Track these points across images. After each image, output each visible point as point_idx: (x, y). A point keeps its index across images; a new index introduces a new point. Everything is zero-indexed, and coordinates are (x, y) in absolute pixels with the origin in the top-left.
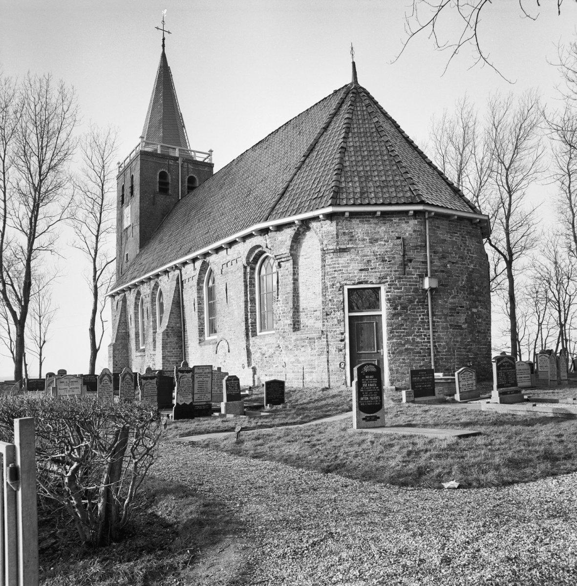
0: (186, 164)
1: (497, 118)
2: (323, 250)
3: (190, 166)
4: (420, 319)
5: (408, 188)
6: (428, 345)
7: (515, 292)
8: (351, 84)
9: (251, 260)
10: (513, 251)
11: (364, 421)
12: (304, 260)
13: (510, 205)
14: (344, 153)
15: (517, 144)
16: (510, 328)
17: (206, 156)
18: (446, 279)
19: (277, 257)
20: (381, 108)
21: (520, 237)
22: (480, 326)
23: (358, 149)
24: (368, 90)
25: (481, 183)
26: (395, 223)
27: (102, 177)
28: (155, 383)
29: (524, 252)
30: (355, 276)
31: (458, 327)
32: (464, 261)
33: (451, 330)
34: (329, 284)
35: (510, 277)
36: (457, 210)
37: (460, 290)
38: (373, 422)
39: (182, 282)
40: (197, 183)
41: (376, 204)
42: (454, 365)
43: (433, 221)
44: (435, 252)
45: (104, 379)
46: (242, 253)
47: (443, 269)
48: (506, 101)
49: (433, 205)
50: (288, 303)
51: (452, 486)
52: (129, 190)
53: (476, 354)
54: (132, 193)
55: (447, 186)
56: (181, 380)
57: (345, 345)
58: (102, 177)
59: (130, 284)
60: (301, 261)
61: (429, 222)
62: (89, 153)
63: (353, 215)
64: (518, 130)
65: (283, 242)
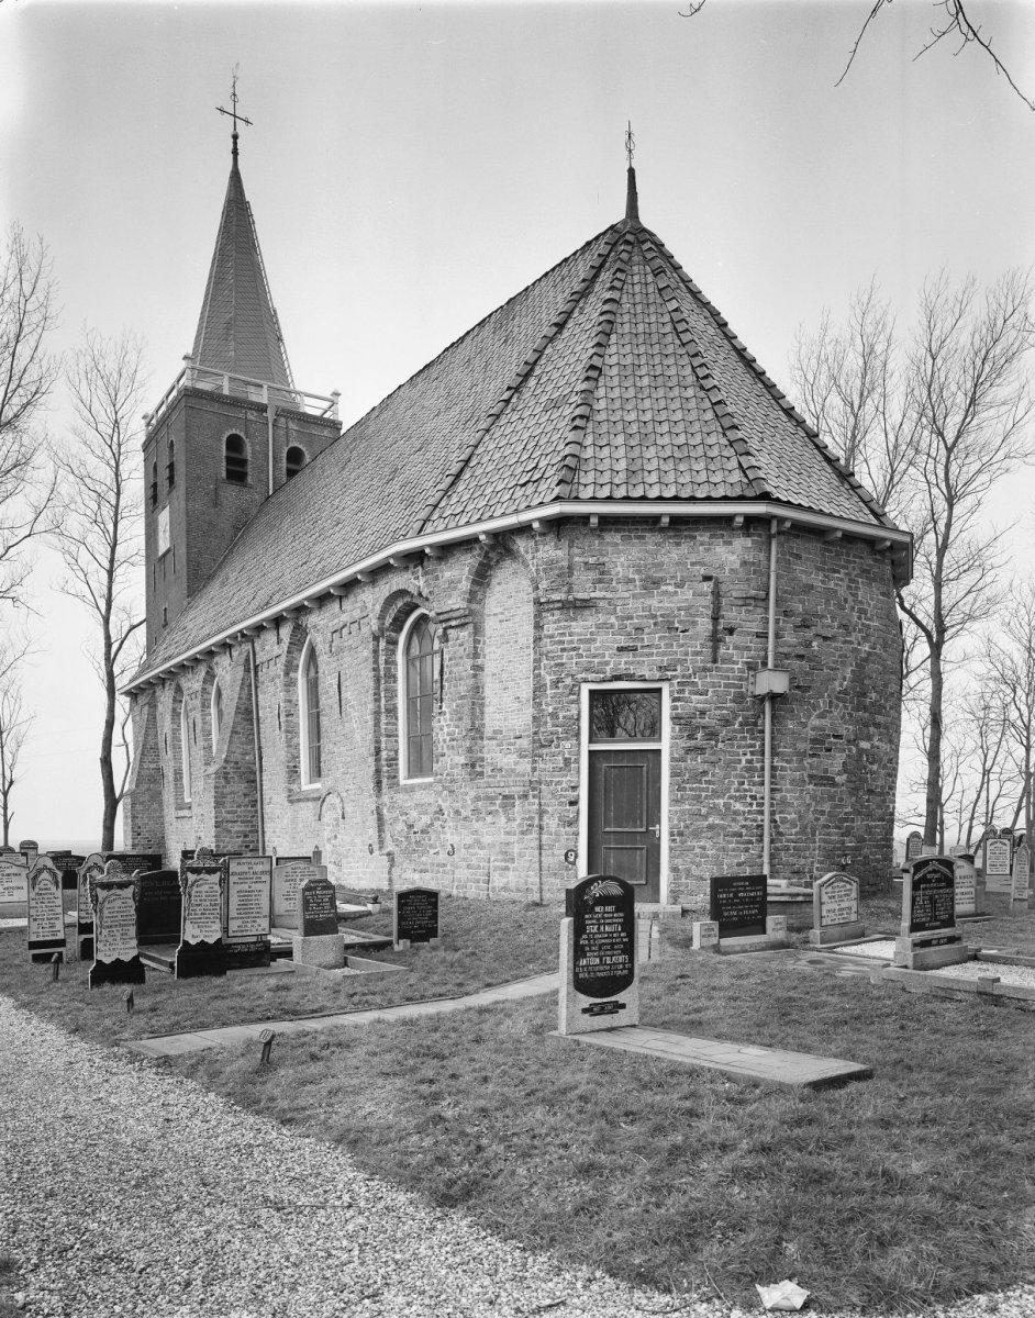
0: (283, 420)
1: (937, 333)
2: (537, 602)
3: (292, 426)
4: (744, 762)
5: (736, 465)
6: (759, 818)
7: (943, 707)
8: (624, 222)
9: (387, 624)
10: (947, 621)
11: (587, 1016)
12: (498, 626)
13: (948, 526)
14: (596, 380)
15: (975, 393)
16: (926, 777)
17: (326, 405)
18: (807, 674)
19: (441, 617)
20: (686, 281)
21: (963, 593)
22: (874, 780)
23: (629, 372)
24: (662, 236)
25: (892, 478)
26: (702, 544)
27: (115, 447)
28: (130, 896)
29: (967, 625)
30: (607, 663)
31: (825, 780)
32: (849, 634)
33: (811, 787)
34: (548, 679)
35: (937, 676)
36: (842, 512)
37: (838, 698)
38: (608, 1017)
39: (256, 667)
40: (307, 458)
41: (660, 499)
42: (812, 863)
43: (788, 540)
44: (785, 614)
45: (40, 879)
46: (370, 606)
47: (802, 652)
48: (960, 298)
49: (788, 504)
50: (460, 719)
51: (784, 1304)
52: (166, 473)
53: (861, 840)
54: (171, 479)
55: (825, 464)
56: (195, 889)
57: (578, 813)
58: (115, 447)
59: (161, 669)
60: (491, 625)
61: (780, 545)
62: (85, 393)
63: (608, 522)
64: (979, 362)
65: (453, 583)
